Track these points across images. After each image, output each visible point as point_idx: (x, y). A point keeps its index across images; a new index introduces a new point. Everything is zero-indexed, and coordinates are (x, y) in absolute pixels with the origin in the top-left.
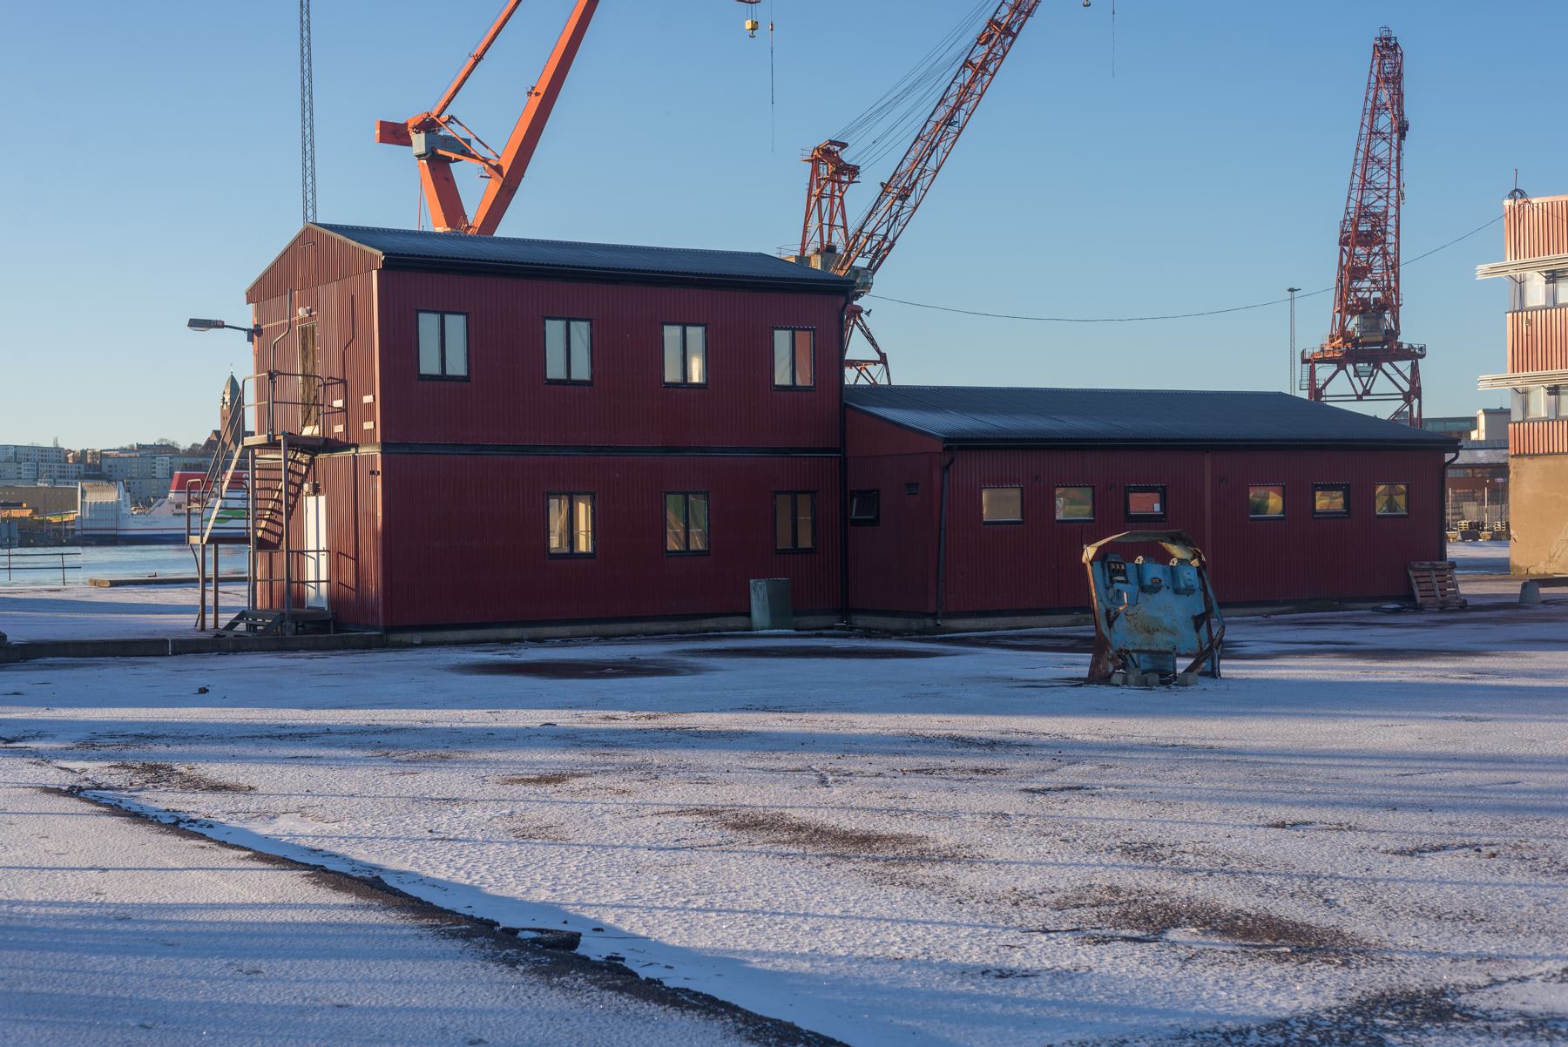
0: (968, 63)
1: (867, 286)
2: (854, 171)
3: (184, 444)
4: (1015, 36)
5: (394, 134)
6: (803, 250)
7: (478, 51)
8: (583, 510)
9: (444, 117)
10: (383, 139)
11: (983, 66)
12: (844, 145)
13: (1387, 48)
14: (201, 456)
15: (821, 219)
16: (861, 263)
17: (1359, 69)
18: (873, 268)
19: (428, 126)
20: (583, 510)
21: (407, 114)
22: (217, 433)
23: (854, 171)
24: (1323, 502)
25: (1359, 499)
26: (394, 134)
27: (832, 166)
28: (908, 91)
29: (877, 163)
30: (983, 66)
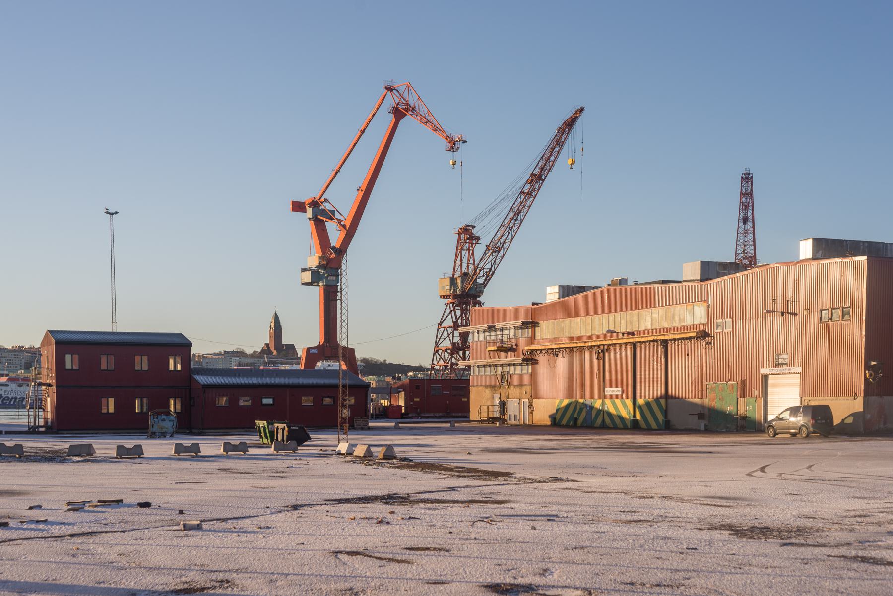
0: (522, 192)
1: (481, 292)
2: (478, 238)
3: (249, 351)
4: (543, 180)
5: (298, 207)
6: (454, 274)
7: (337, 168)
8: (145, 400)
9: (323, 199)
10: (294, 210)
11: (530, 194)
12: (474, 227)
13: (747, 178)
14: (258, 357)
15: (461, 261)
16: (480, 281)
17: (736, 187)
18: (485, 284)
19: (315, 204)
20: (145, 400)
21: (305, 198)
22: (267, 345)
23: (478, 238)
24: (266, 401)
25: (233, 401)
26: (298, 207)
27: (468, 236)
28: (497, 205)
29: (486, 234)
30: (530, 194)
